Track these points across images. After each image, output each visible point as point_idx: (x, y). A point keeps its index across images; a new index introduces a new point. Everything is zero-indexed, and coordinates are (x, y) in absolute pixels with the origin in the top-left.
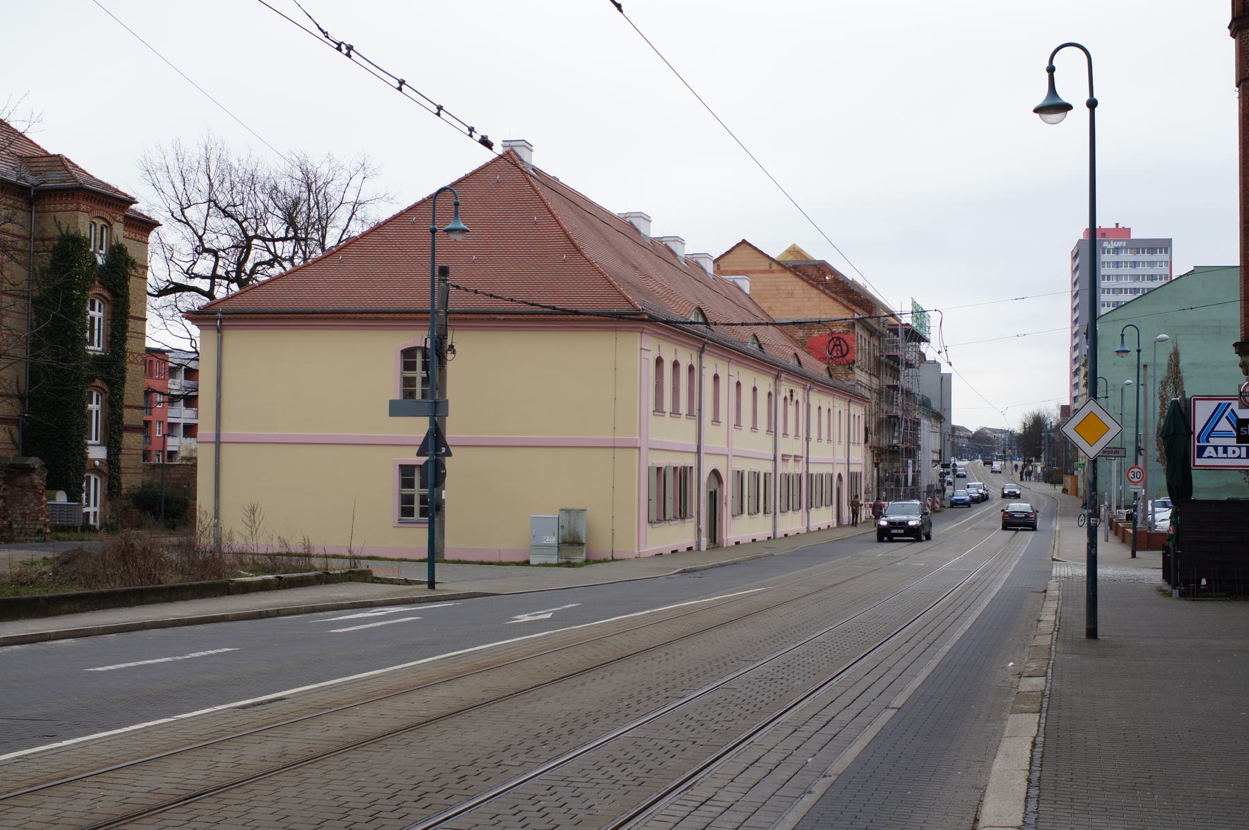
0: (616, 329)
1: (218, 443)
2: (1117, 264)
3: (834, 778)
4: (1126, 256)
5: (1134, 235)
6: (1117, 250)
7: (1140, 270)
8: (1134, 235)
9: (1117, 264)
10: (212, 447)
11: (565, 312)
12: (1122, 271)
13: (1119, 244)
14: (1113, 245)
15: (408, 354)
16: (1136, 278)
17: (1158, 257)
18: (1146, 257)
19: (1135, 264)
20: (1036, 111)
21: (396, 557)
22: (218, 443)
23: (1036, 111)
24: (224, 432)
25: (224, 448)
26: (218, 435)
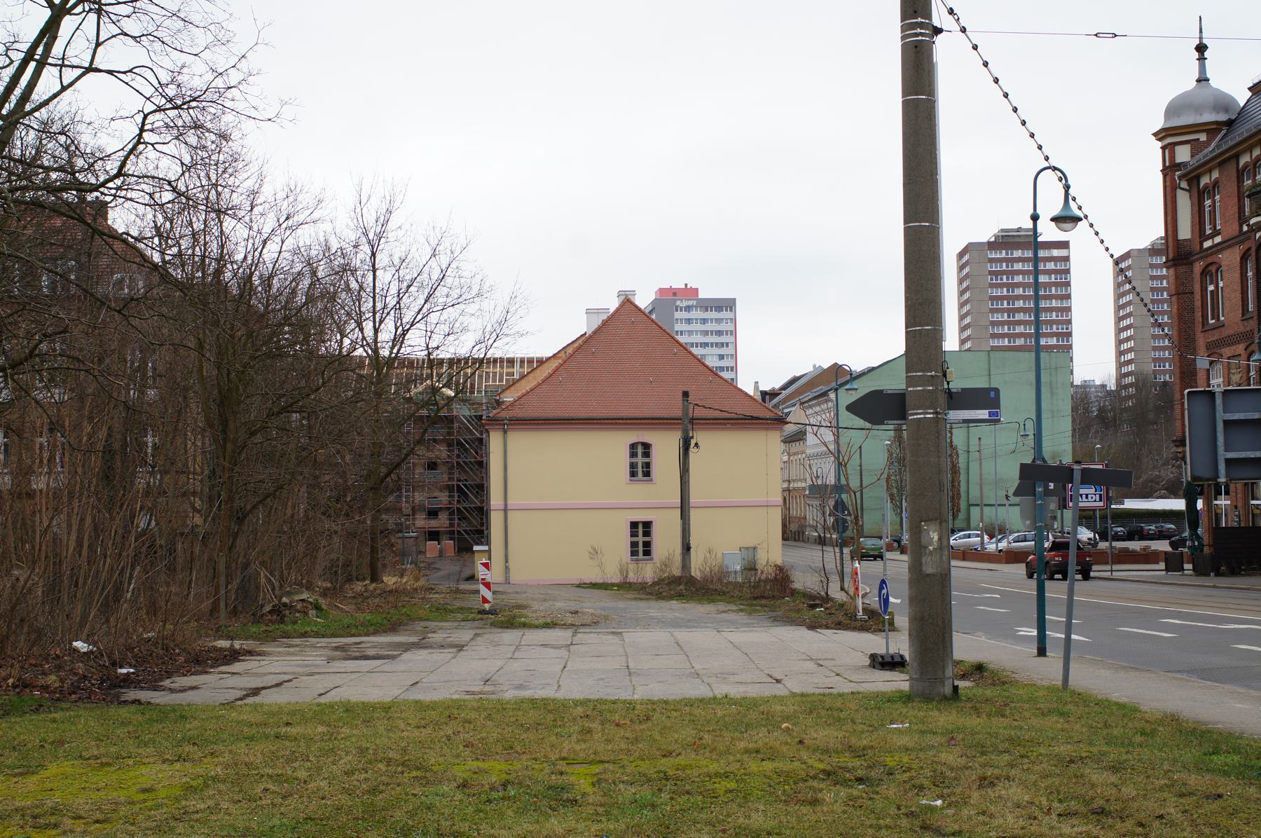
0: (767, 429)
1: (506, 510)
2: (689, 321)
3: (784, 692)
4: (697, 314)
5: (702, 295)
6: (688, 308)
7: (709, 327)
8: (702, 295)
9: (689, 321)
10: (502, 513)
11: (753, 418)
12: (694, 327)
13: (690, 303)
14: (685, 303)
15: (633, 446)
16: (706, 333)
17: (725, 314)
18: (713, 315)
19: (704, 321)
20: (1052, 220)
21: (510, 564)
22: (506, 510)
23: (1052, 220)
24: (509, 502)
25: (510, 514)
26: (506, 505)
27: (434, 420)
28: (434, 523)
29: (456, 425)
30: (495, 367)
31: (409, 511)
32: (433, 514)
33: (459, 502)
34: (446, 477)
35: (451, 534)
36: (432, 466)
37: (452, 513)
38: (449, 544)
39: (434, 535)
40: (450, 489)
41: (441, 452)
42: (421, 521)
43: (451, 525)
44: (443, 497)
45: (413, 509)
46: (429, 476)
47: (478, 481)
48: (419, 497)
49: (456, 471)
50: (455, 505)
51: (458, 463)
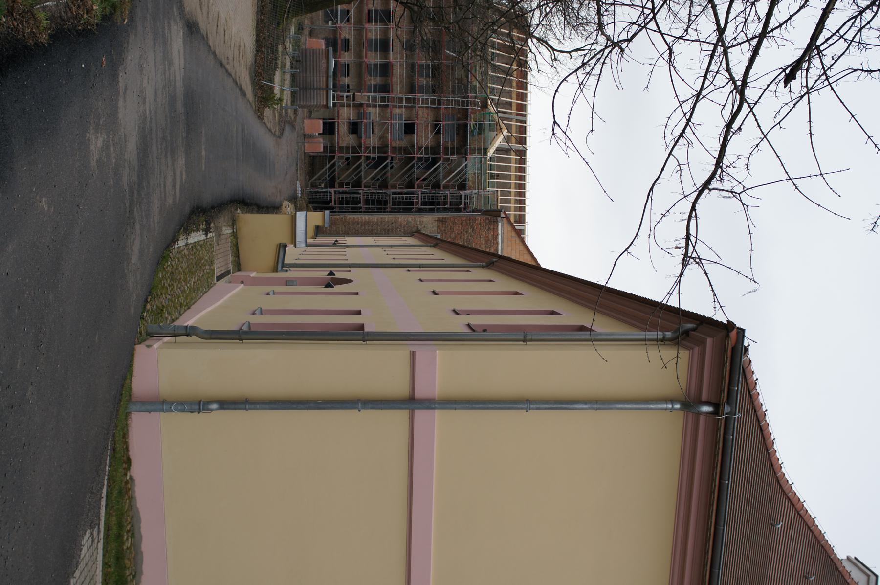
1: (411, 402)
10: (398, 387)
22: (411, 402)
24: (438, 415)
25: (402, 416)
26: (429, 404)
27: (462, 131)
28: (343, 128)
29: (455, 157)
30: (516, 209)
31: (358, 101)
32: (354, 128)
33: (367, 158)
34: (397, 144)
35: (330, 149)
36: (409, 128)
37: (354, 150)
38: (318, 146)
39: (329, 128)
40: (383, 148)
41: (424, 138)
42: (346, 114)
43: (341, 149)
44: (373, 141)
45: (361, 105)
46: (397, 124)
47: (391, 182)
48: (373, 112)
49: (403, 156)
50: (364, 154)
51: (386, 158)
